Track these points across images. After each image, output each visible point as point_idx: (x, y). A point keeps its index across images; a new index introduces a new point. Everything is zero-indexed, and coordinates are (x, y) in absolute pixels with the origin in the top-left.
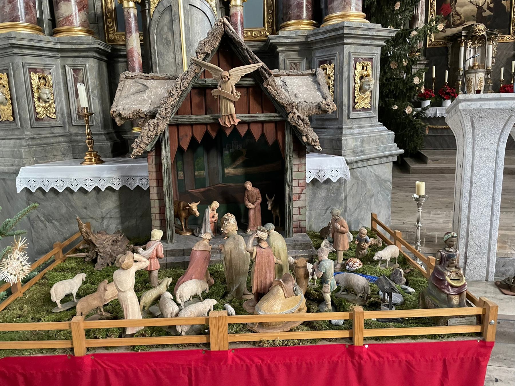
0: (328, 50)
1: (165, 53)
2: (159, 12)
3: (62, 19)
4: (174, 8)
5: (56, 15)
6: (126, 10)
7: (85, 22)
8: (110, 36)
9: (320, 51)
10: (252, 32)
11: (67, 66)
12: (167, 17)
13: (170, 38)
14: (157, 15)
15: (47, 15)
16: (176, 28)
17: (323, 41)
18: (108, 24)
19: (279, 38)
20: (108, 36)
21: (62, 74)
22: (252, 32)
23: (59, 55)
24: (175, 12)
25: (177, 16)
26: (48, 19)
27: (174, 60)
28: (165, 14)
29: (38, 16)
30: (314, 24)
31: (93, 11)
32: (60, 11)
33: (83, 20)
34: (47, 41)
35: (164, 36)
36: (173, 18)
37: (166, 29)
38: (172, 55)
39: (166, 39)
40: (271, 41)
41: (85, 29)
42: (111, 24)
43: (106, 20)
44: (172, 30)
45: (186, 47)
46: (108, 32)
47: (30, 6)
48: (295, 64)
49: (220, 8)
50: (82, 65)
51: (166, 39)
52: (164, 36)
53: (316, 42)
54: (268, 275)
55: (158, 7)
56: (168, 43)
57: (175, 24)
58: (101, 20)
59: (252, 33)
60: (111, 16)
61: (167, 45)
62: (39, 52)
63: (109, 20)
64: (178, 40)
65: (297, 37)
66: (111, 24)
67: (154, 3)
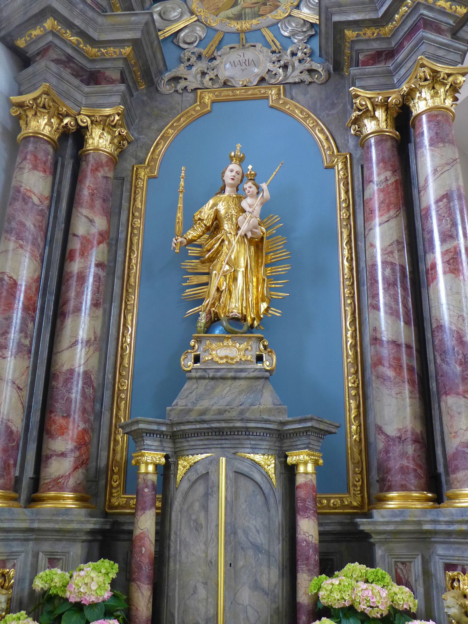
0: (458, 548)
1: (191, 542)
2: (189, 480)
3: (49, 480)
4: (212, 477)
5: (42, 475)
6: (141, 476)
7: (80, 484)
8: (113, 500)
9: (444, 546)
10: (329, 500)
11: (41, 555)
12: (200, 489)
13: (202, 520)
14: (185, 485)
15: (29, 472)
16: (212, 506)
17: (449, 534)
18: (113, 483)
19: (375, 523)
20: (110, 500)
21: (32, 565)
22: (329, 500)
23: (34, 537)
24: (213, 482)
25: (215, 489)
26: (30, 478)
27: (204, 555)
28: (198, 483)
29: (17, 474)
30: (430, 497)
31: (94, 464)
32: (48, 470)
33: (78, 482)
34: (22, 518)
35: (194, 517)
36: (210, 491)
37: (197, 506)
38: (203, 547)
39: (196, 521)
40: (362, 528)
41: (78, 495)
42: (117, 483)
43: (111, 478)
44: (205, 508)
45: (225, 536)
46: (111, 494)
47: (9, 465)
48: (403, 563)
49: (281, 473)
50: (64, 553)
51: (196, 521)
52: (194, 517)
53: (435, 533)
54: (418, 506)
55: (189, 474)
56: (198, 527)
57: (212, 500)
58: (104, 476)
59: (329, 501)
60: (119, 473)
61: (197, 530)
62: (5, 534)
63: (115, 477)
64: (214, 524)
65: (404, 522)
66: (117, 483)
67: (184, 467)
